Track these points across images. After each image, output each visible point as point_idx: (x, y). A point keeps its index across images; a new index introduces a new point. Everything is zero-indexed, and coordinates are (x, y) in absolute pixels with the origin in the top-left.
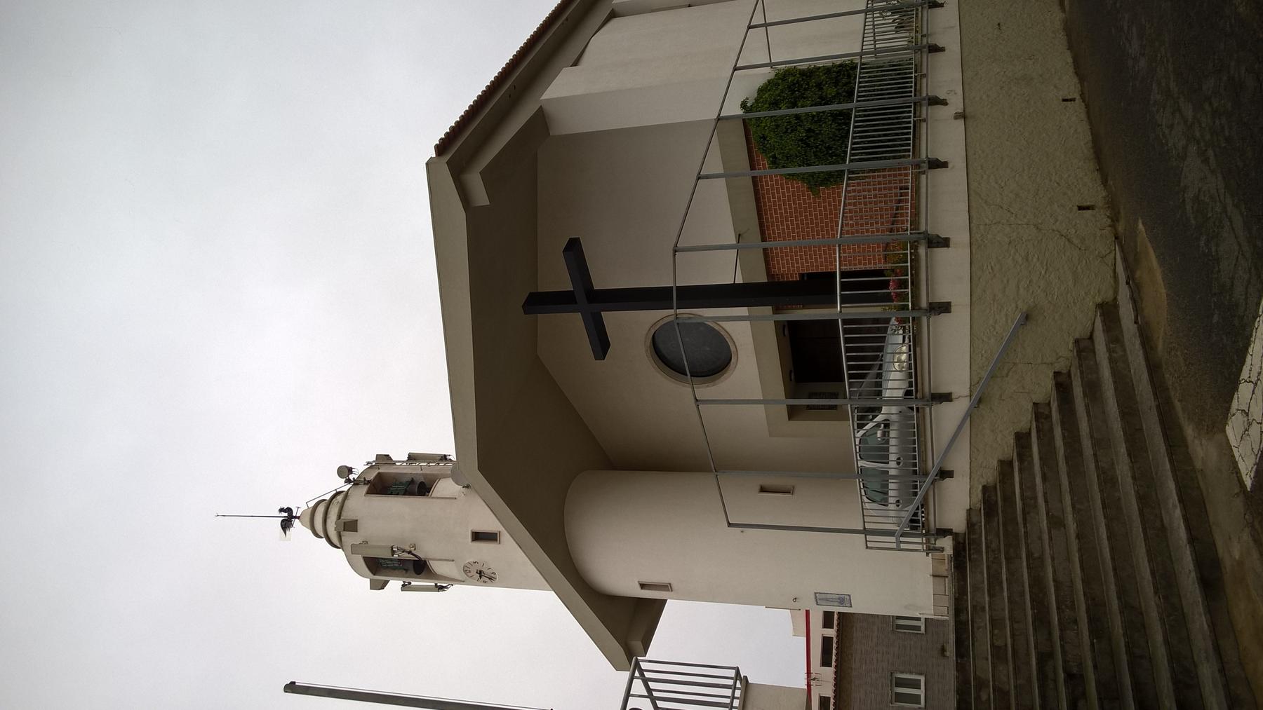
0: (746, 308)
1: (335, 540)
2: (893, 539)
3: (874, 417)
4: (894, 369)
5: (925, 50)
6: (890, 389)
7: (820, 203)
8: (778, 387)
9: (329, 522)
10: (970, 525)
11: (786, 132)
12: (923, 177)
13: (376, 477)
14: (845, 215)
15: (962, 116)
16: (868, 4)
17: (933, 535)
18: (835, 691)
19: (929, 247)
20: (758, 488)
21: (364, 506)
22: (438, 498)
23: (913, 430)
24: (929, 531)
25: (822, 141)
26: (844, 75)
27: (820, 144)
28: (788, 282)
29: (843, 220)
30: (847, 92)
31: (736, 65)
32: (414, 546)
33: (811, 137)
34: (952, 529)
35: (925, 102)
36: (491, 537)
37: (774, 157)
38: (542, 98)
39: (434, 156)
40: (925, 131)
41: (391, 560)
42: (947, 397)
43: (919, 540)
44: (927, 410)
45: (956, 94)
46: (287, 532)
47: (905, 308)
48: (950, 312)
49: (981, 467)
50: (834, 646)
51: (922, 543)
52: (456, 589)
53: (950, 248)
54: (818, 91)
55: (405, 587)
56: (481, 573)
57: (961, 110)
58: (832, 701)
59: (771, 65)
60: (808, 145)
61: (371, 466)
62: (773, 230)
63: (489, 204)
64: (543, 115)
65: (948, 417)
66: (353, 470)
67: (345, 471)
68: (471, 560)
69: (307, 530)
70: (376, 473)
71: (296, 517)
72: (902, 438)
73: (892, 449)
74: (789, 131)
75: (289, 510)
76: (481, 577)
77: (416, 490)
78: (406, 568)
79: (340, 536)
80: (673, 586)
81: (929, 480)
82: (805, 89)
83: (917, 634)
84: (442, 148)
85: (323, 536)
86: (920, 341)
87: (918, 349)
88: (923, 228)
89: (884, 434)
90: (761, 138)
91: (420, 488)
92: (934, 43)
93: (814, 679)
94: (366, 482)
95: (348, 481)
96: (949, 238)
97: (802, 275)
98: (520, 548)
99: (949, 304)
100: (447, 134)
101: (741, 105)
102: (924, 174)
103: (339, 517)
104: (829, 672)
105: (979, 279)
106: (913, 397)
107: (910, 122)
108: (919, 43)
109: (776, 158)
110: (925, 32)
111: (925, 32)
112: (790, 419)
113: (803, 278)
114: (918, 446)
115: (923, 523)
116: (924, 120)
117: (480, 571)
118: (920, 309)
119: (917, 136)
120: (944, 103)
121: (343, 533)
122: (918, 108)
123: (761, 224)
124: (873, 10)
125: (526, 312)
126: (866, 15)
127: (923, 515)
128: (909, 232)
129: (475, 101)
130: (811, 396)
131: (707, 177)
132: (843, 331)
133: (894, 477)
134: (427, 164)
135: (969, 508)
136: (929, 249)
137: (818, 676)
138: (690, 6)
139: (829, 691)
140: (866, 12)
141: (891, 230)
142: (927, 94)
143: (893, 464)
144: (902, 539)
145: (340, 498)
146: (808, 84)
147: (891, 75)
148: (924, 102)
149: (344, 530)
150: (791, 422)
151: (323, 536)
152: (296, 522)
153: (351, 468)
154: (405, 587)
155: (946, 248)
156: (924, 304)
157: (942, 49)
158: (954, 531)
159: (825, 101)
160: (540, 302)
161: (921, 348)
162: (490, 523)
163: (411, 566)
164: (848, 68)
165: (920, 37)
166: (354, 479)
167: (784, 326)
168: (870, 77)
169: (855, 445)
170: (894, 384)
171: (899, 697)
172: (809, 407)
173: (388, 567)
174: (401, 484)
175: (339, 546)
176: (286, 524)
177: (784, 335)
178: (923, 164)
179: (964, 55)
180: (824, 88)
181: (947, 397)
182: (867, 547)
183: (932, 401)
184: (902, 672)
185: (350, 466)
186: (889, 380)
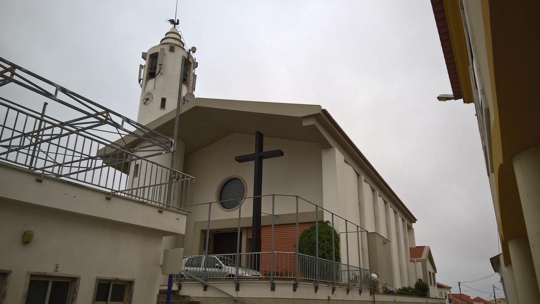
1: (165, 41)
7: (291, 247)
8: (213, 227)
9: (173, 40)
10: (184, 297)
13: (190, 62)
15: (329, 299)
17: (179, 283)
19: (294, 284)
21: (179, 55)
24: (181, 281)
34: (181, 290)
35: (333, 286)
36: (163, 105)
38: (336, 148)
42: (237, 289)
45: (335, 297)
46: (169, 21)
47: (274, 275)
48: (271, 291)
49: (208, 301)
55: (141, 66)
56: (147, 99)
57: (331, 299)
61: (194, 60)
62: (279, 229)
63: (303, 125)
64: (329, 148)
65: (230, 289)
67: (194, 50)
69: (170, 30)
71: (175, 26)
72: (214, 273)
74: (320, 238)
75: (178, 23)
81: (204, 282)
84: (325, 111)
85: (166, 36)
87: (258, 279)
94: (188, 58)
95: (190, 50)
99: (274, 290)
103: (176, 45)
105: (282, 301)
107: (328, 281)
110: (353, 288)
112: (202, 230)
116: (328, 286)
117: (148, 99)
119: (324, 283)
120: (333, 293)
123: (281, 225)
129: (343, 130)
130: (209, 239)
132: (248, 254)
134: (320, 106)
135: (190, 296)
136: (293, 284)
138: (359, 204)
145: (182, 45)
148: (334, 286)
150: (200, 230)
152: (173, 26)
154: (141, 66)
155: (293, 290)
156: (275, 282)
157: (348, 294)
158: (180, 291)
160: (260, 137)
161: (258, 280)
163: (152, 71)
166: (190, 53)
169: (213, 256)
172: (205, 239)
173: (152, 61)
175: (162, 43)
176: (172, 22)
179: (346, 301)
181: (237, 289)
185: (196, 52)
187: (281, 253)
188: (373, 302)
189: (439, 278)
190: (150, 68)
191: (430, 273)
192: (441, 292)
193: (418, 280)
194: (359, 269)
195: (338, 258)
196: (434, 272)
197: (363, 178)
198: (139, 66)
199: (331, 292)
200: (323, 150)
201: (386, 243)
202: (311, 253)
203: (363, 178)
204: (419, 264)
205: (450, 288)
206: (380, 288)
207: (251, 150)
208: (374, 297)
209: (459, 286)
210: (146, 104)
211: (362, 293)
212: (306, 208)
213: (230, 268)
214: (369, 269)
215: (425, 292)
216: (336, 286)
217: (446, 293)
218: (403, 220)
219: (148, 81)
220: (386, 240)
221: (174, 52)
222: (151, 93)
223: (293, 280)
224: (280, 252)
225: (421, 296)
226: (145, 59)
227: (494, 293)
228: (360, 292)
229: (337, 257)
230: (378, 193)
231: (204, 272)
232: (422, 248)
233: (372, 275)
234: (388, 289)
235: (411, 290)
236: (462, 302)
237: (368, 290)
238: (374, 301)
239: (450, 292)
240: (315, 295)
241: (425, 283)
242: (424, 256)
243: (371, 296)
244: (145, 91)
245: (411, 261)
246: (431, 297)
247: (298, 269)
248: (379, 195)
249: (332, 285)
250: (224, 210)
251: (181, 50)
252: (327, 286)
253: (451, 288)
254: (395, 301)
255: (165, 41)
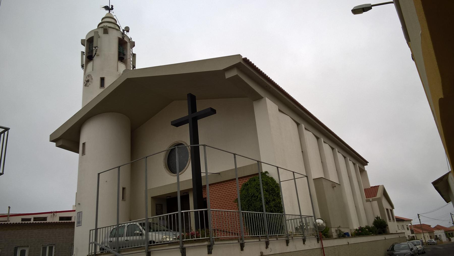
0: (192, 178)
1: (101, 26)
2: (94, 241)
3: (144, 229)
4: (163, 236)
5: (287, 239)
6: (155, 234)
7: (232, 203)
11: (257, 188)
12: (237, 241)
14: (226, 212)
16: (304, 216)
18: (49, 223)
20: (124, 187)
21: (114, 37)
22: (118, 64)
23: (130, 246)
25: (254, 202)
26: (278, 209)
27: (252, 202)
28: (202, 192)
29: (232, 211)
30: (272, 210)
31: (236, 154)
32: (98, 56)
33: (255, 198)
35: (267, 240)
36: (102, 84)
37: (248, 185)
38: (266, 98)
39: (243, 57)
40: (255, 241)
41: (93, 47)
43: (93, 251)
44: (144, 251)
45: (271, 251)
50: (68, 221)
51: (92, 253)
52: (82, 71)
53: (207, 254)
54: (272, 200)
55: (83, 53)
56: (88, 81)
58: (45, 222)
59: (280, 182)
60: (252, 197)
61: (130, 39)
66: (128, 32)
67: (127, 29)
68: (93, 77)
70: (127, 41)
71: (109, 11)
73: (132, 238)
75: (112, 9)
76: (86, 81)
77: (121, 56)
78: (90, 53)
79: (102, 27)
80: (84, 156)
82: (273, 195)
83: (71, 254)
84: (246, 60)
85: (102, 21)
86: (170, 245)
87: (167, 245)
88: (215, 243)
89: (138, 234)
90: (254, 179)
91: (122, 58)
92: (290, 241)
93: (54, 214)
94: (123, 38)
95: (124, 31)
96: (212, 254)
97: (206, 198)
98: (98, 96)
100: (273, 81)
101: (266, 171)
102: (238, 242)
104: (57, 220)
106: (149, 244)
108: (290, 236)
109: (247, 185)
110: (294, 238)
111: (294, 238)
113: (205, 199)
114: (130, 248)
115: (103, 252)
116: (260, 240)
118: (183, 244)
119: (253, 238)
120: (267, 247)
121: (103, 28)
122: (264, 237)
123: (224, 182)
124: (301, 218)
125: (188, 95)
126: (300, 215)
127: (106, 252)
128: (214, 237)
131: (235, 157)
133: (118, 239)
134: (240, 55)
137: (55, 216)
138: (302, 152)
139: (49, 220)
140: (301, 215)
141: (214, 230)
142: (270, 241)
143: (126, 238)
144: (93, 244)
145: (117, 28)
146: (274, 195)
147: (279, 227)
148: (267, 239)
149: (104, 29)
150: (151, 198)
151: (102, 21)
152: (108, 12)
153: (129, 32)
154: (83, 53)
155: (207, 253)
156: (185, 246)
157: (287, 245)
159: (267, 203)
160: (192, 100)
162: (107, 84)
163: (90, 54)
164: (281, 210)
165: (292, 236)
166: (125, 33)
167: (187, 193)
168: (278, 218)
170: (154, 236)
171: (45, 249)
174: (123, 51)
175: (99, 27)
176: (107, 8)
177: (184, 193)
178: (242, 241)
179: (285, 254)
180: (273, 202)
182: (90, 230)
183: (147, 252)
184: (55, 249)
185: (129, 31)
186: (159, 234)
187: (212, 210)
188: (321, 249)
189: (397, 213)
190: (88, 52)
191: (387, 210)
192: (402, 225)
193: (376, 218)
194: (299, 217)
195: (280, 208)
196: (391, 209)
197: (303, 126)
198: (81, 52)
199: (264, 246)
200: (254, 102)
201: (335, 187)
202: (250, 206)
203: (303, 126)
204: (375, 203)
205: (410, 220)
206: (333, 232)
207: (185, 113)
208: (322, 243)
209: (419, 217)
210: (87, 86)
211: (306, 242)
212: (242, 163)
213: (154, 234)
214: (313, 216)
215: (384, 229)
216: (269, 240)
217: (408, 225)
218: (354, 164)
219: (87, 64)
220: (335, 184)
221: (108, 34)
222: (91, 75)
223: (207, 241)
224: (212, 209)
225: (380, 233)
226: (84, 45)
227: (452, 219)
228: (304, 241)
229: (279, 207)
230: (322, 140)
231: (126, 242)
232: (376, 188)
233: (317, 221)
234: (342, 232)
235: (367, 230)
236: (423, 232)
237: (314, 237)
238: (323, 248)
239: (411, 224)
240: (241, 253)
241: (383, 220)
242: (379, 194)
243: (318, 242)
244: (86, 73)
245: (367, 201)
246: (391, 232)
247: (243, 224)
248: (324, 142)
249: (266, 238)
250: (172, 175)
251: (115, 31)
252: (258, 241)
253: (412, 220)
254: (348, 244)
255: (101, 26)
